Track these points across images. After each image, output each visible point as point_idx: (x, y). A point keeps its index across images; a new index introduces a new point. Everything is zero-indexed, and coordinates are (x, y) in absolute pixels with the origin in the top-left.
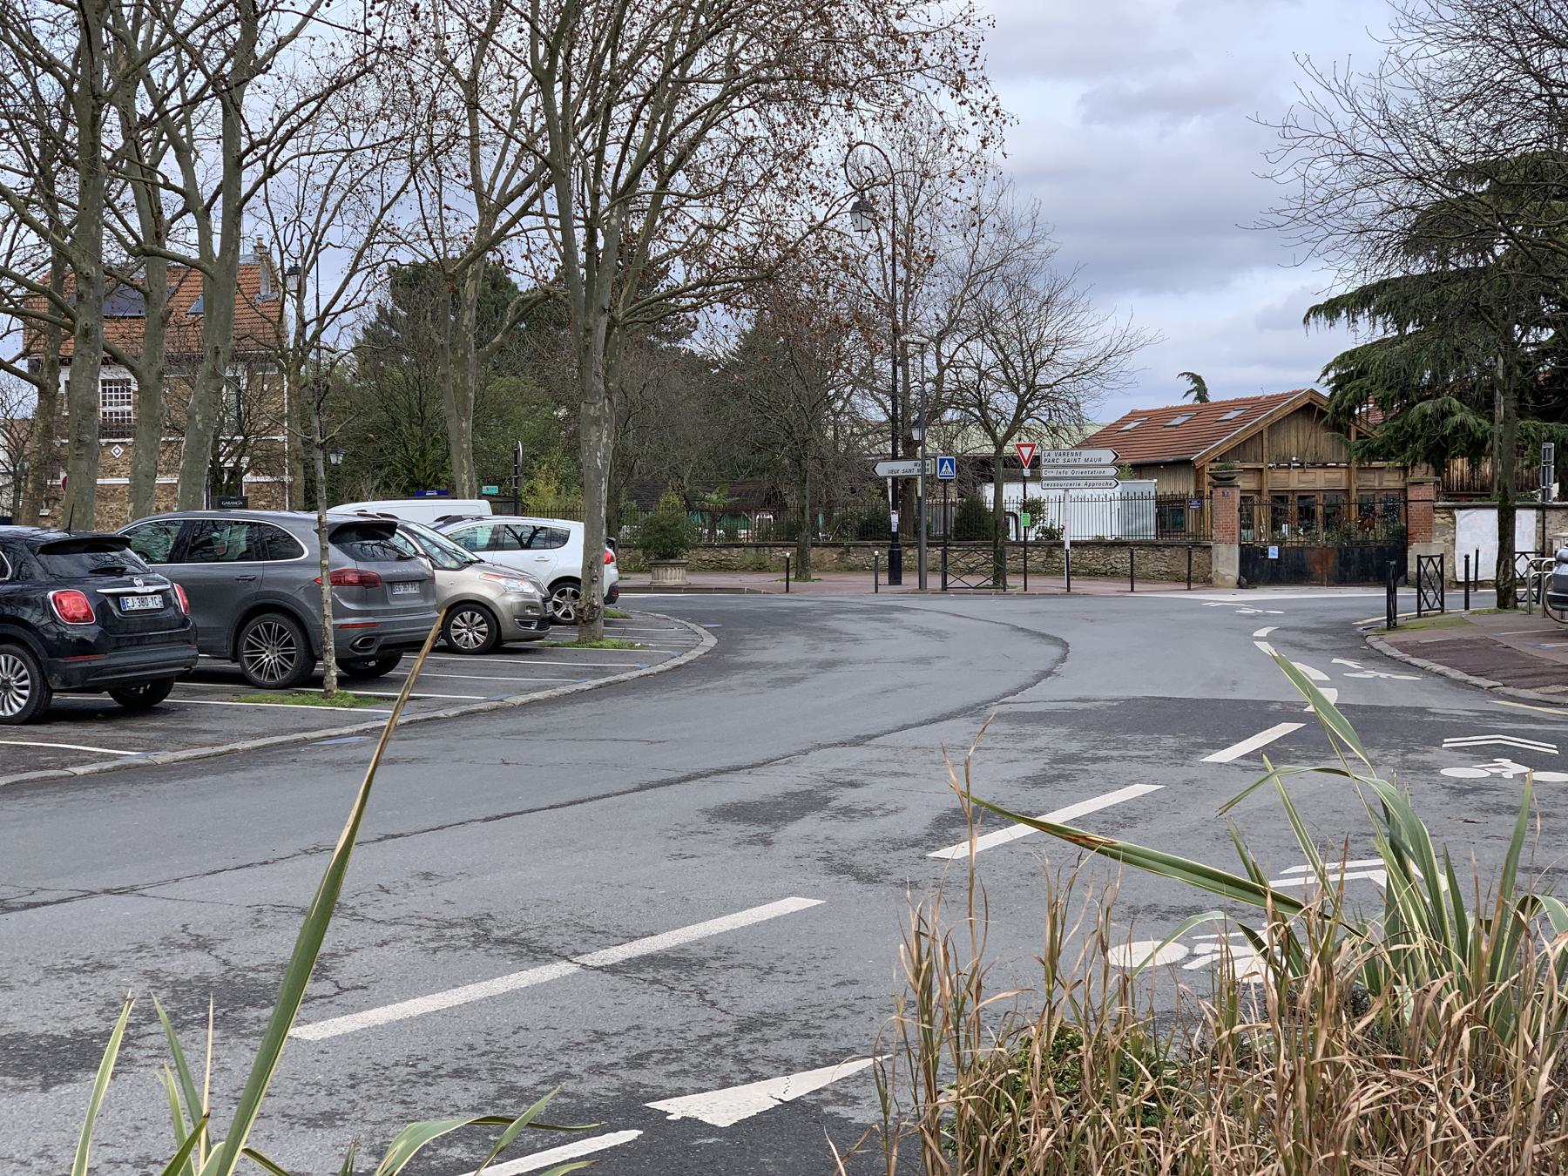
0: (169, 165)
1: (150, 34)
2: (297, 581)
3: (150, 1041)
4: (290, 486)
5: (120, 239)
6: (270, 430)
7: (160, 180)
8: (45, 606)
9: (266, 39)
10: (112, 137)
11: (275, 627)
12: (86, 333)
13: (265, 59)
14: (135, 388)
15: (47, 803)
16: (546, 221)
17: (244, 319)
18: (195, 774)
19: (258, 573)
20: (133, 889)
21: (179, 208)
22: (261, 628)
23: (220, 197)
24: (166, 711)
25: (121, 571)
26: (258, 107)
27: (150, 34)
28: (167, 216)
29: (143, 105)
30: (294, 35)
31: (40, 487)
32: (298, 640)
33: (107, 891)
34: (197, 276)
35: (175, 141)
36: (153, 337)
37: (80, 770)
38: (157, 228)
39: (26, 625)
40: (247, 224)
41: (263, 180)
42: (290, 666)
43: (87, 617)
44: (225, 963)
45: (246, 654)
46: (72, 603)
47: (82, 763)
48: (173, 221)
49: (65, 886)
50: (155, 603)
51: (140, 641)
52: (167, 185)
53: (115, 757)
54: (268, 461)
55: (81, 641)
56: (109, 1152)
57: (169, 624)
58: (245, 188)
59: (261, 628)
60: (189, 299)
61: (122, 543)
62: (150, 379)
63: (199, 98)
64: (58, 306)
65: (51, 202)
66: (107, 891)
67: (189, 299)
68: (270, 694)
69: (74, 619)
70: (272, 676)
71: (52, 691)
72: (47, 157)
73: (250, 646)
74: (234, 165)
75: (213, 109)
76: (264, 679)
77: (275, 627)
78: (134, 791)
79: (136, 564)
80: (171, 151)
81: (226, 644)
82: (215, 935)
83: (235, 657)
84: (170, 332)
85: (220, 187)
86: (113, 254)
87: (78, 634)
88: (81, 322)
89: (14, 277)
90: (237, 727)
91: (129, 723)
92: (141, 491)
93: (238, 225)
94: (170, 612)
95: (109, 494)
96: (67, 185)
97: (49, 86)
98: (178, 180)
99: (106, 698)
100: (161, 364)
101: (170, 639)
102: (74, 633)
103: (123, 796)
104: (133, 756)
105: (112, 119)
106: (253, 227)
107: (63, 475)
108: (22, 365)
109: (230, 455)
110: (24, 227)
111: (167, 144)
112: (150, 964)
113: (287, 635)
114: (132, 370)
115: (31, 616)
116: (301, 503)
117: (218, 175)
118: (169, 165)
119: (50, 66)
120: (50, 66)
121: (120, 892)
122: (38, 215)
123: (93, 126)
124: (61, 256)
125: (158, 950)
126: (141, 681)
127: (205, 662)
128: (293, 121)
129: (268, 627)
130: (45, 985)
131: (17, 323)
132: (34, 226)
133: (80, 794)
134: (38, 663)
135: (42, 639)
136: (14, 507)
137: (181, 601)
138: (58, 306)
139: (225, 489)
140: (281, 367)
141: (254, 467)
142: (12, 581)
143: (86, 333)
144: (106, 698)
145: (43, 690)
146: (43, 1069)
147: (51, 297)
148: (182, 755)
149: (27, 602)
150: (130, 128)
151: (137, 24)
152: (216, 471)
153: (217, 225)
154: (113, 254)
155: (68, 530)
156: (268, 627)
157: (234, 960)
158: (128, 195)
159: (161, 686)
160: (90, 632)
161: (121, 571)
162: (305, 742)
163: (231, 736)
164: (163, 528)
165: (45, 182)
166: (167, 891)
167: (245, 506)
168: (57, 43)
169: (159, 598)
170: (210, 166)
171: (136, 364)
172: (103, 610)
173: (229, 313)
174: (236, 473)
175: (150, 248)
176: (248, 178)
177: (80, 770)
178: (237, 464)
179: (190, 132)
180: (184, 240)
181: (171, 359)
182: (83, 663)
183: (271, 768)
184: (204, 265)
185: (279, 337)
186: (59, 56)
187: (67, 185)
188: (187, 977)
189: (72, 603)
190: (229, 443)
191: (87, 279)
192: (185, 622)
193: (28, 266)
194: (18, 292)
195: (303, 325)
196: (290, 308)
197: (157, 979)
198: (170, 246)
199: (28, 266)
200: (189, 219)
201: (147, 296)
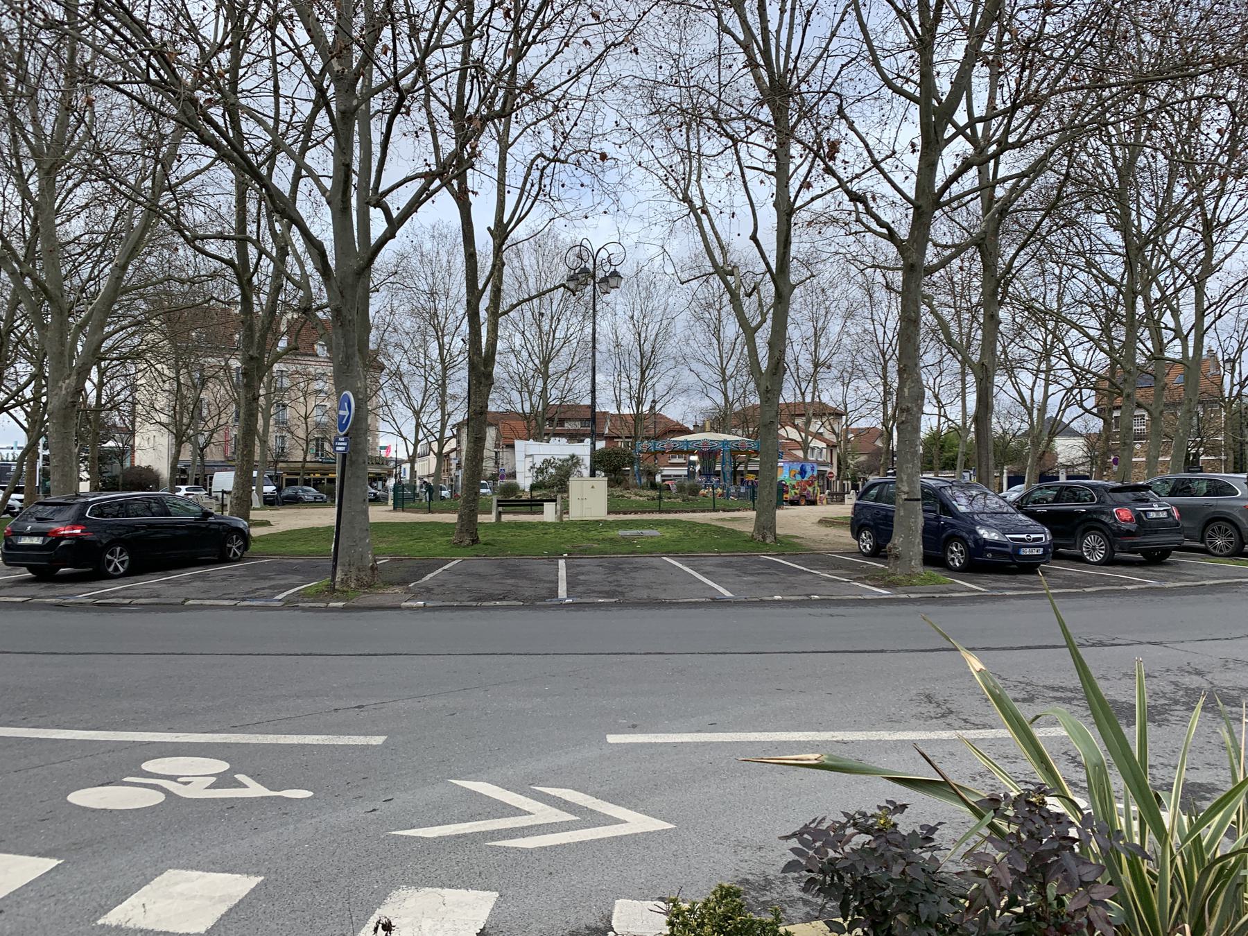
0: (1168, 319)
1: (1158, 262)
2: (1235, 507)
3: (1176, 713)
4: (1226, 460)
5: (1143, 353)
6: (1215, 434)
7: (1163, 326)
8: (1112, 514)
9: (1218, 256)
10: (1140, 308)
11: (1223, 528)
12: (1128, 396)
13: (1217, 265)
14: (1146, 418)
15: (1116, 601)
16: (981, 119)
17: (1204, 384)
18: (157, 611)
19: (1214, 503)
20: (1161, 643)
21: (1171, 337)
22: (1216, 528)
23: (1193, 331)
24: (1168, 564)
25: (1148, 501)
26: (1213, 287)
27: (1158, 262)
28: (1165, 341)
29: (1156, 294)
30: (1233, 251)
31: (1104, 463)
32: (1235, 534)
33: (1149, 643)
34: (1180, 367)
35: (1170, 307)
36: (1158, 396)
37: (1129, 588)
38: (1160, 347)
39: (1103, 522)
40: (1206, 340)
41: (1214, 322)
42: (1231, 547)
43: (1131, 520)
44: (1211, 683)
45: (1208, 540)
46: (1124, 514)
47: (1131, 584)
48: (1168, 343)
49: (1129, 638)
50: (1164, 515)
51: (1156, 532)
52: (1166, 328)
53: (1146, 583)
54: (1213, 449)
55: (1128, 531)
56: (1161, 760)
57: (1170, 525)
58: (1206, 325)
59: (1216, 528)
60: (1175, 377)
61: (1146, 488)
62: (1156, 414)
63: (1182, 287)
64: (1113, 384)
65: (1110, 340)
66: (1149, 643)
67: (1175, 377)
68: (1220, 559)
69: (1125, 521)
70: (1221, 551)
71: (1114, 552)
72: (1109, 320)
73: (1210, 536)
74: (1200, 315)
75: (1191, 292)
76: (1217, 552)
77: (1223, 528)
78: (1156, 599)
79: (1153, 497)
80: (1168, 312)
81: (1197, 534)
82: (1204, 669)
83: (1202, 541)
84: (1166, 392)
85: (1193, 326)
86: (1140, 360)
87: (1127, 528)
88: (1126, 391)
89: (1092, 373)
90: (1204, 573)
91: (1151, 568)
92: (1151, 464)
93: (1202, 342)
94: (1171, 519)
95: (1137, 464)
96: (1120, 333)
97: (1111, 291)
98: (1172, 325)
99: (1139, 556)
100: (1162, 407)
101: (1170, 532)
102: (1125, 527)
103: (1151, 600)
104: (1154, 583)
105: (1140, 301)
106: (1209, 341)
107: (1113, 457)
108: (1095, 411)
109: (1194, 447)
110: (1098, 351)
111: (1167, 308)
112: (1173, 678)
113: (1230, 532)
114: (1147, 410)
115: (1105, 518)
116: (1232, 469)
117: (1193, 320)
118: (1168, 319)
119: (1111, 282)
120: (1111, 282)
121: (1155, 643)
122: (1106, 346)
123: (1132, 306)
124: (1114, 362)
125: (1177, 673)
126: (1157, 549)
127: (1188, 543)
128: (1232, 292)
129: (1220, 528)
130: (1124, 681)
131: (1093, 393)
132: (1102, 350)
133: (1131, 598)
134: (1109, 539)
135: (1110, 529)
136: (1091, 472)
137: (1176, 514)
138: (1113, 384)
139: (1192, 463)
140: (1221, 406)
141: (1206, 453)
142: (1097, 503)
143: (1128, 396)
144: (1139, 556)
145: (1111, 551)
146: (1126, 718)
147: (1110, 380)
148: (1178, 584)
149: (1103, 513)
150: (1148, 305)
151: (1153, 256)
152: (1188, 454)
153: (1191, 343)
154: (1140, 360)
155: (1122, 482)
156: (1220, 528)
157: (1216, 683)
158: (1147, 333)
159: (1167, 552)
160: (1133, 527)
161: (1148, 501)
162: (1241, 583)
163: (1202, 578)
164: (1165, 481)
165: (1106, 330)
166: (1178, 646)
167: (1201, 471)
168: (1113, 271)
169: (1165, 513)
170: (1188, 316)
171: (1149, 408)
172: (1138, 517)
173: (1197, 382)
174: (1197, 455)
175: (1158, 355)
176: (1207, 321)
177: (1129, 588)
178: (1197, 451)
179: (1178, 303)
180: (1174, 350)
181: (1166, 405)
182: (1129, 540)
183: (1225, 595)
184: (1185, 362)
185: (1221, 392)
186: (1115, 277)
187: (1120, 333)
188: (1192, 687)
189: (1124, 514)
190: (1193, 441)
191: (1129, 372)
192: (1178, 524)
193: (1099, 368)
194: (1094, 380)
195: (1233, 385)
196: (1227, 378)
197: (1177, 685)
198: (1167, 355)
199: (1099, 368)
200: (1177, 341)
201: (1155, 378)
